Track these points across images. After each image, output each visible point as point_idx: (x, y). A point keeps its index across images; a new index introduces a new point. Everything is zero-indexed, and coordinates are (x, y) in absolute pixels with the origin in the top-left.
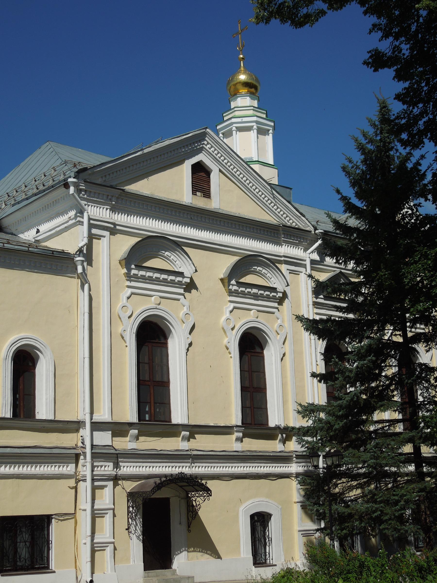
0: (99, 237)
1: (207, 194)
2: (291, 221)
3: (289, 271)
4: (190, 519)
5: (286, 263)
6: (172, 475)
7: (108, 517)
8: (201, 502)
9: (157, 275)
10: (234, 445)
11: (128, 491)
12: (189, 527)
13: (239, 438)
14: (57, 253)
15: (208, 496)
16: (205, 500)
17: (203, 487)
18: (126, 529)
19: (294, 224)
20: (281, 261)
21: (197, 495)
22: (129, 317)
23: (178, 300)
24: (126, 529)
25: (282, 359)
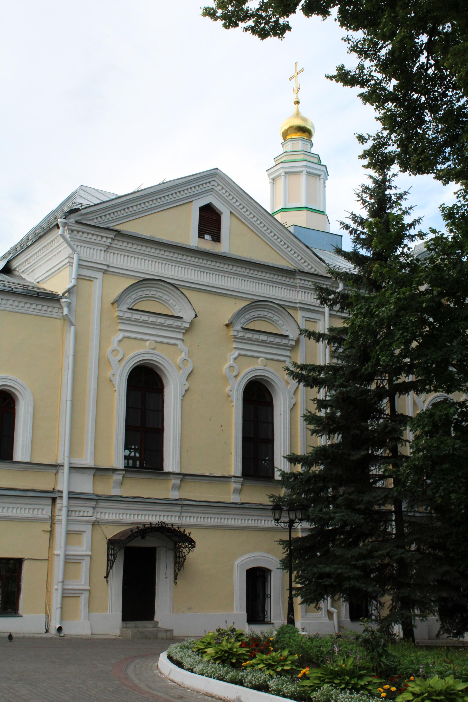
0: (90, 279)
1: (217, 238)
2: (310, 267)
3: (305, 319)
4: (177, 570)
5: (302, 309)
6: (151, 524)
7: (85, 565)
8: (186, 553)
9: (271, 339)
10: (232, 497)
11: (109, 538)
12: (176, 579)
13: (237, 489)
14: (43, 294)
15: (192, 548)
16: (189, 552)
17: (186, 538)
18: (105, 577)
19: (313, 270)
20: (297, 307)
21: (183, 546)
22: (236, 376)
23: (176, 345)
24: (105, 577)
25: (291, 410)
